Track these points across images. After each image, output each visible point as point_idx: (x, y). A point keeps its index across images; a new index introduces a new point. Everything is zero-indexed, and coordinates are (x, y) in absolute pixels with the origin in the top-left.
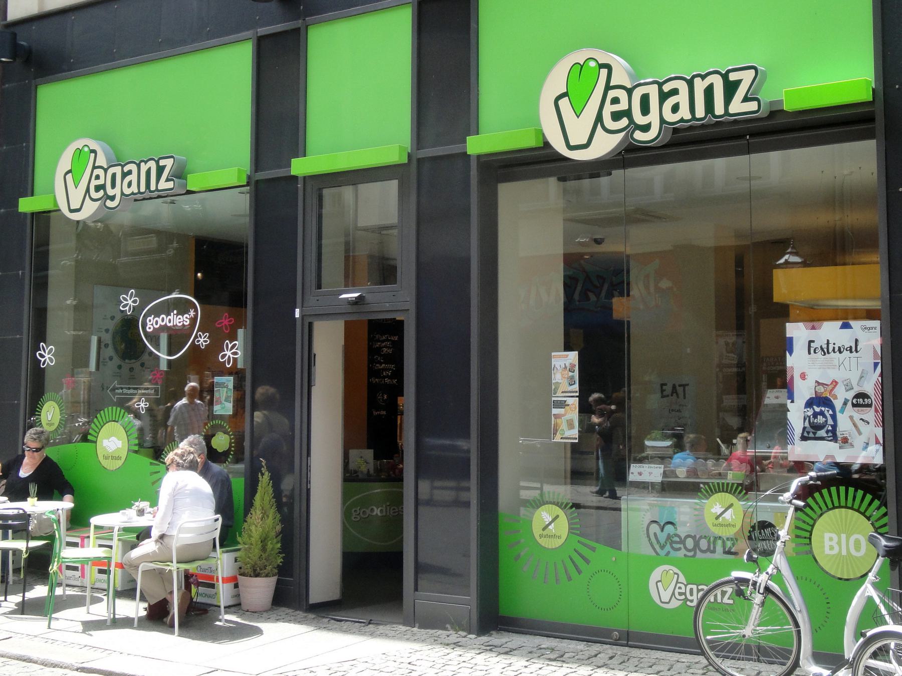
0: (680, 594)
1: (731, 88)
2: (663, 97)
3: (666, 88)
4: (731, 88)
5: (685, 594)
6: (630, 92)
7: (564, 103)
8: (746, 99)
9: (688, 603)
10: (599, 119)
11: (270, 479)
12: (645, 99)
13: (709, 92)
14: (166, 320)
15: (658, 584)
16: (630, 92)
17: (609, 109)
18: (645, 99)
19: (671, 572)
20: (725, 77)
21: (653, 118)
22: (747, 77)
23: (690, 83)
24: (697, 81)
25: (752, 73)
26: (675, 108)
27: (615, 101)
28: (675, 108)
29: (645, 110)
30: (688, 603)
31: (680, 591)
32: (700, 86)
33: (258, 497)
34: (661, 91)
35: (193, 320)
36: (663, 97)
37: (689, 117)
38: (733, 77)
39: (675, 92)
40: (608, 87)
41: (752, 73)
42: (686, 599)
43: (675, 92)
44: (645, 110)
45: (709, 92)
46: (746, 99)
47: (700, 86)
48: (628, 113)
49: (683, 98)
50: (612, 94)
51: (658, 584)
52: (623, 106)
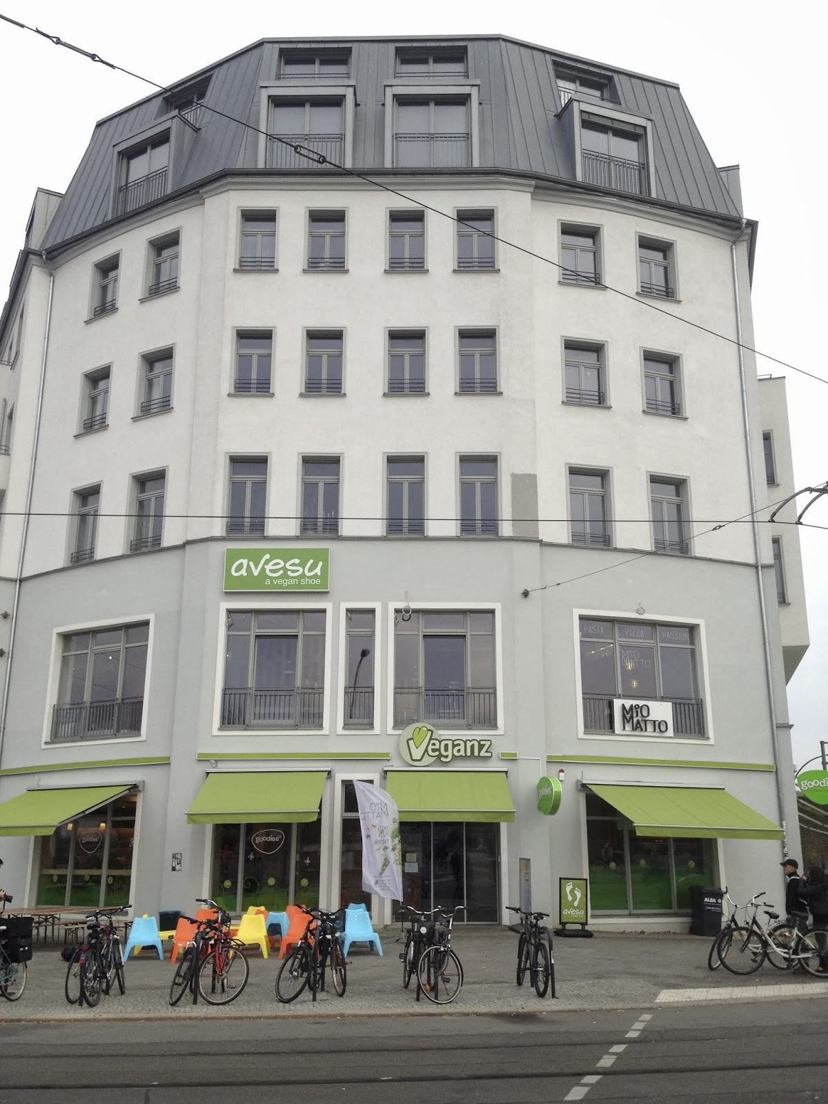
0: (434, 750)
1: (481, 747)
2: (454, 746)
3: (455, 743)
4: (481, 747)
5: (439, 750)
6: (440, 742)
7: (411, 742)
8: (486, 752)
9: (443, 759)
10: (426, 750)
11: (297, 853)
12: (446, 746)
13: (472, 746)
14: (267, 839)
15: (409, 742)
16: (440, 742)
17: (430, 747)
18: (446, 746)
19: (425, 729)
20: (479, 742)
21: (449, 753)
22: (488, 744)
23: (465, 742)
24: (468, 742)
25: (489, 742)
26: (459, 751)
27: (434, 744)
28: (459, 751)
29: (446, 750)
30: (443, 759)
31: (433, 747)
32: (469, 744)
33: (367, 874)
34: (453, 743)
35: (280, 840)
36: (454, 746)
37: (464, 755)
38: (482, 743)
39: (459, 745)
40: (431, 739)
41: (489, 742)
42: (440, 755)
43: (459, 745)
44: (446, 750)
45: (472, 746)
46: (486, 752)
47: (469, 744)
48: (439, 750)
49: (462, 747)
50: (432, 742)
51: (409, 742)
52: (437, 747)
